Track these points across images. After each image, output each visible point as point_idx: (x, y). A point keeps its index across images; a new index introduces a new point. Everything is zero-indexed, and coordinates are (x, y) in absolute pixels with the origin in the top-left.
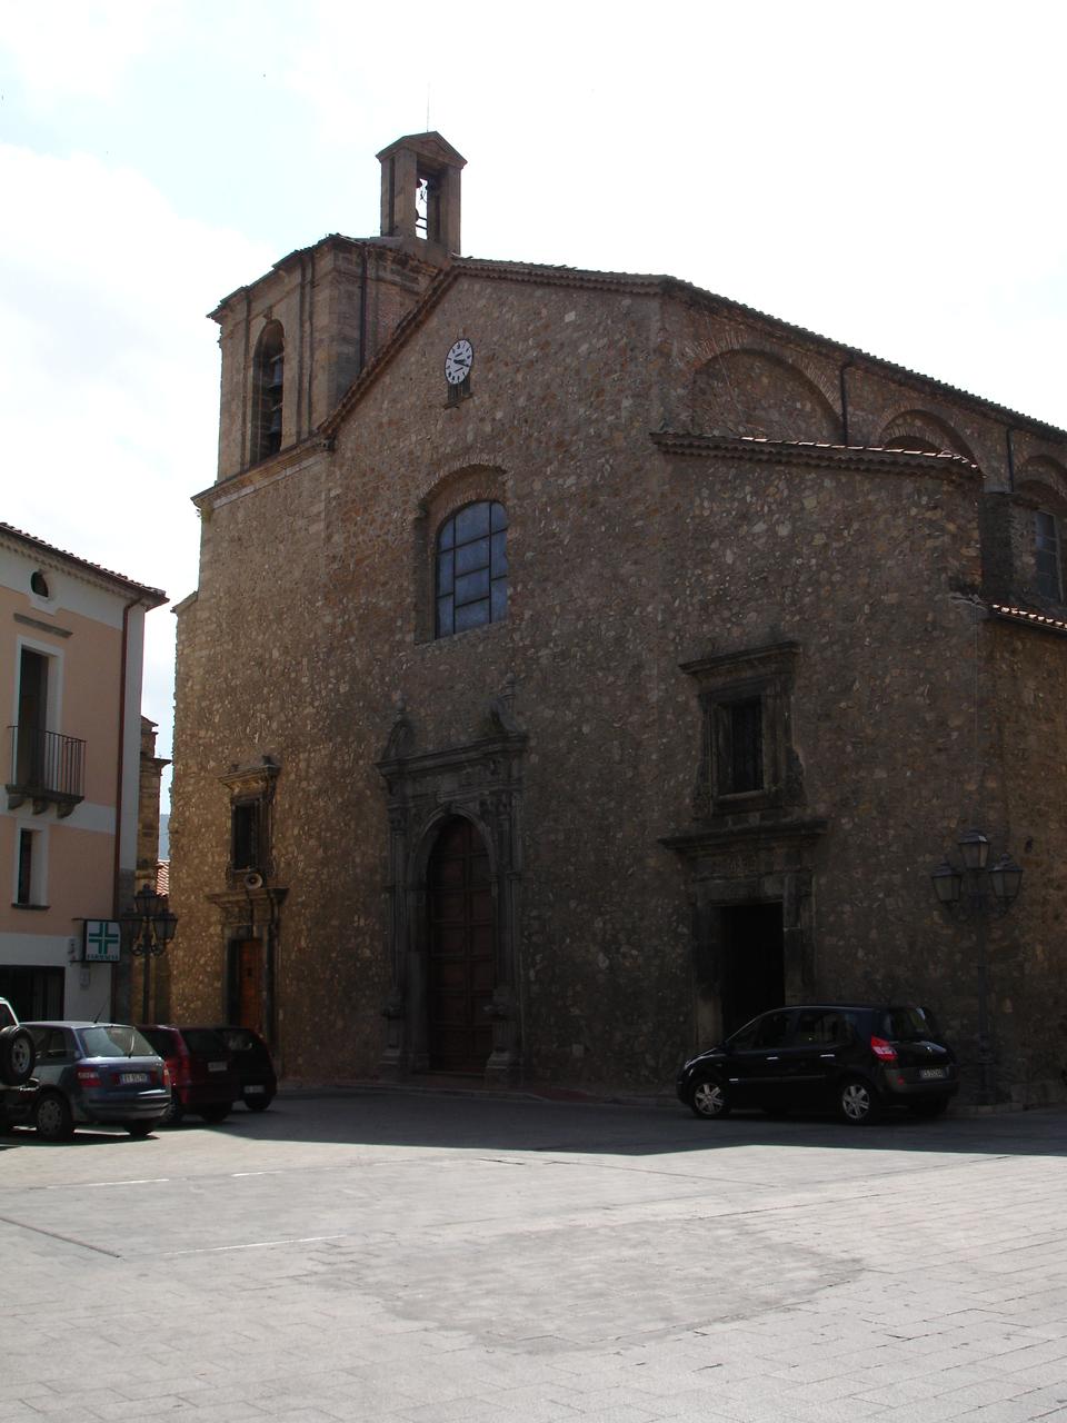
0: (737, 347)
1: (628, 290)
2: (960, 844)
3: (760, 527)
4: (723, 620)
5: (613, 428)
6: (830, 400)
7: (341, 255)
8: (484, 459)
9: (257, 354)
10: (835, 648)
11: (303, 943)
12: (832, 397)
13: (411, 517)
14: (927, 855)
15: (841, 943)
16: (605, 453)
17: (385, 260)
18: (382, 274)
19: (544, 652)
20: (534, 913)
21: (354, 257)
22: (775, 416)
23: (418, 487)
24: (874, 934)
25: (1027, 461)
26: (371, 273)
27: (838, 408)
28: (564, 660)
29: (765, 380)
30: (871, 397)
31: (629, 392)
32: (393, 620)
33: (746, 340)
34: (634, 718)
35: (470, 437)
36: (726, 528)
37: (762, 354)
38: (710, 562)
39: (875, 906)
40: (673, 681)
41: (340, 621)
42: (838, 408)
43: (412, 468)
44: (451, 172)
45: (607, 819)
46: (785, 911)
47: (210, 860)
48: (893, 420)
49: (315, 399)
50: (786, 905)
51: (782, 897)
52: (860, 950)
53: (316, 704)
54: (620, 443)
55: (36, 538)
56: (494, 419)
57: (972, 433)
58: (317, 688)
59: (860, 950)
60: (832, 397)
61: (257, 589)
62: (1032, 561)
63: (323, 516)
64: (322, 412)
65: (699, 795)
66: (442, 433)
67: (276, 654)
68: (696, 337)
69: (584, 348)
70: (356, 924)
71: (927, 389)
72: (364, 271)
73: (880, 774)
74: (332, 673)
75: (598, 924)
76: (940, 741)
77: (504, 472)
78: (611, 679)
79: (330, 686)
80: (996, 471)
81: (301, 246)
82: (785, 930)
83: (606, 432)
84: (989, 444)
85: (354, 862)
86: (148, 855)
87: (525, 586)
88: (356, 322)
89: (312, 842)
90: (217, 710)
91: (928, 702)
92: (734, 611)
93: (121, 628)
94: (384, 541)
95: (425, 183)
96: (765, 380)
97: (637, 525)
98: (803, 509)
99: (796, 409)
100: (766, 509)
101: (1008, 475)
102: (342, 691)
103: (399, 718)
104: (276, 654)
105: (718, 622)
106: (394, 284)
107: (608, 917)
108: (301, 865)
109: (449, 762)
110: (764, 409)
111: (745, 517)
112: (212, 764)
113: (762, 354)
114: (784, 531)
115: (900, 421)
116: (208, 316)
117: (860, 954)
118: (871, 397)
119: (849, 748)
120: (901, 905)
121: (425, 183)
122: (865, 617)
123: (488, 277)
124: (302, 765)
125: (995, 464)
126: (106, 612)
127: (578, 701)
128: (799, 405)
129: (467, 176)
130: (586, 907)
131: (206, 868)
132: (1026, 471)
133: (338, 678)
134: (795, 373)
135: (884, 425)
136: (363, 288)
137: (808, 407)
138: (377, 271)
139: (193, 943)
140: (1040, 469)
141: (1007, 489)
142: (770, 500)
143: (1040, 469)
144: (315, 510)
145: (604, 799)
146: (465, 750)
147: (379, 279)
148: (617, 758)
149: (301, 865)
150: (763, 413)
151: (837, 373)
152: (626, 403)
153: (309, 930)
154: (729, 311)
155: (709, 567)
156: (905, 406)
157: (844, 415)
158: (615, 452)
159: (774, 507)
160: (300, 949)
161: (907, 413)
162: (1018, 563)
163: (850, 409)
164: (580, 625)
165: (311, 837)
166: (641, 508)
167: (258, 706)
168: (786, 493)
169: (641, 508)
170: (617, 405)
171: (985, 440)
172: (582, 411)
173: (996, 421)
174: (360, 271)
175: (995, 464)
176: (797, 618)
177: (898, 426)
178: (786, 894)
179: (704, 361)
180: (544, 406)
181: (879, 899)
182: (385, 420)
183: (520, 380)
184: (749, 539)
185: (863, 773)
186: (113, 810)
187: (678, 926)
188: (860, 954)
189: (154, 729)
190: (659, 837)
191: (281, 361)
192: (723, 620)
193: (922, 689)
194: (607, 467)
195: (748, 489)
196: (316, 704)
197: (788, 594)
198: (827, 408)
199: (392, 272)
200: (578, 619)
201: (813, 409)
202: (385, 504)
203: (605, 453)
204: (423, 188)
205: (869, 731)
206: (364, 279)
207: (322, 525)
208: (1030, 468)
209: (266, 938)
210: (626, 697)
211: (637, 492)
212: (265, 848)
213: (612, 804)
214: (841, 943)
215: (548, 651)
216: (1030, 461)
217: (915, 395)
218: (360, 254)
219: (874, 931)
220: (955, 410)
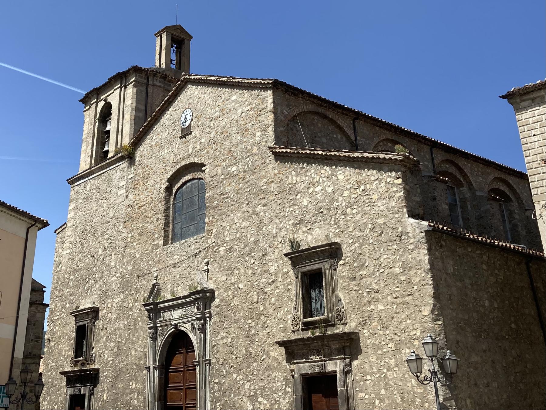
0: (306, 110)
1: (258, 86)
2: (423, 343)
3: (318, 189)
4: (303, 232)
5: (253, 145)
6: (349, 134)
7: (138, 74)
8: (196, 160)
9: (100, 116)
10: (356, 245)
11: (105, 398)
12: (350, 132)
13: (164, 187)
14: (407, 349)
15: (367, 396)
16: (249, 156)
17: (157, 77)
18: (155, 82)
19: (222, 248)
20: (217, 381)
21: (143, 75)
22: (324, 140)
23: (167, 173)
24: (383, 392)
25: (441, 162)
26: (150, 82)
27: (353, 137)
28: (231, 252)
29: (320, 125)
30: (368, 133)
31: (259, 129)
32: (154, 234)
33: (310, 107)
34: (263, 280)
35: (190, 151)
36: (303, 189)
37: (317, 113)
38: (296, 205)
39: (382, 376)
40: (281, 262)
41: (130, 235)
42: (353, 137)
43: (164, 165)
44: (186, 42)
45: (251, 331)
46: (338, 379)
47: (64, 354)
48: (378, 143)
49: (124, 135)
50: (338, 376)
51: (335, 371)
52: (377, 400)
53: (117, 275)
54: (255, 151)
55: (23, 211)
56: (201, 142)
57: (415, 149)
58: (118, 267)
59: (377, 400)
60: (350, 132)
61: (94, 221)
62: (447, 207)
63: (125, 187)
64: (126, 141)
65: (294, 319)
66: (178, 148)
67: (100, 251)
68: (288, 106)
69: (240, 111)
70: (130, 387)
71: (393, 130)
72: (148, 81)
73: (381, 307)
74: (125, 260)
75: (247, 386)
76: (409, 290)
77: (205, 166)
78: (252, 261)
79: (124, 266)
80: (427, 167)
81: (121, 71)
82: (339, 389)
83: (249, 147)
84: (422, 154)
85: (131, 354)
86: (35, 352)
87: (214, 217)
88: (144, 102)
89: (112, 344)
90: (72, 279)
91: (401, 271)
92: (308, 228)
93: (25, 238)
94: (151, 198)
95: (175, 46)
96: (320, 125)
97: (263, 188)
98: (338, 180)
99: (334, 137)
100: (321, 180)
101: (433, 168)
102: (129, 268)
103: (155, 282)
104: (100, 251)
105: (301, 233)
106: (160, 87)
107: (252, 383)
108: (106, 356)
109: (177, 303)
110: (319, 137)
111: (312, 184)
112: (68, 305)
113: (317, 113)
114: (329, 190)
115: (381, 144)
116: (80, 101)
117: (377, 402)
118: (368, 133)
119: (365, 294)
120: (395, 376)
121: (175, 46)
122: (369, 230)
123: (199, 82)
124: (109, 306)
125: (426, 163)
126: (19, 228)
127: (237, 272)
128: (335, 136)
129: (193, 43)
130: (241, 377)
131: (61, 358)
132: (441, 166)
133: (128, 263)
134: (333, 122)
135: (374, 145)
136: (147, 88)
137: (339, 137)
138: (153, 81)
139: (52, 398)
140: (447, 166)
141: (432, 174)
142: (322, 176)
143: (447, 166)
144: (121, 184)
145: (250, 321)
146: (185, 297)
147: (154, 85)
148: (255, 300)
149: (106, 356)
150: (319, 139)
151: (351, 122)
152: (258, 134)
153: (108, 390)
154: (302, 95)
155: (296, 207)
156: (383, 137)
157: (356, 140)
158: (254, 155)
159: (325, 179)
160: (103, 401)
161: (384, 140)
162: (440, 208)
163: (358, 138)
164: (238, 235)
165: (111, 342)
166: (265, 180)
167: (91, 277)
168: (330, 173)
169: (265, 180)
170: (254, 135)
171: (421, 152)
172: (239, 138)
173: (425, 144)
174: (145, 81)
175: (426, 163)
176: (338, 230)
177: (380, 145)
178: (338, 370)
179: (292, 116)
180: (222, 136)
181: (384, 373)
182: (154, 143)
183: (212, 125)
184: (314, 194)
185: (372, 307)
186: (14, 327)
187: (285, 388)
188: (377, 402)
189: (44, 289)
190: (276, 340)
191: (110, 119)
192: (303, 232)
193: (398, 264)
194: (250, 162)
195: (313, 171)
196: (117, 275)
197: (333, 219)
198: (348, 138)
199: (160, 82)
200: (237, 233)
201: (342, 138)
202: (152, 181)
203: (249, 156)
204: (174, 48)
205: (374, 285)
206: (147, 85)
207: (124, 191)
208: (442, 165)
209: (87, 395)
210: (260, 270)
211: (263, 173)
212: (90, 348)
213: (253, 324)
214: (367, 396)
215: (224, 248)
216: (442, 162)
217: (387, 132)
218: (147, 74)
219: (383, 390)
220: (406, 139)
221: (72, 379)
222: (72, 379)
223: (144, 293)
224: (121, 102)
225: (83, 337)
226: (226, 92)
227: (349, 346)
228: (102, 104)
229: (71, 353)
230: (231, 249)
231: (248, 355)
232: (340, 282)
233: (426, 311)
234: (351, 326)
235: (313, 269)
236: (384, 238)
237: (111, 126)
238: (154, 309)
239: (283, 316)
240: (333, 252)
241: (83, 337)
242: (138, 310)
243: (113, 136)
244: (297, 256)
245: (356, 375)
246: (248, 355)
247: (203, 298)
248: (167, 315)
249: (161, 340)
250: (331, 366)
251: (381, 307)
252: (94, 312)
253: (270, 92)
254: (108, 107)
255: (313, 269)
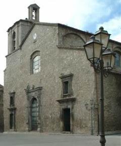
73: (82, 91)
111: (67, 57)
212: (14, 102)
221: (11, 110)
222: (11, 110)
223: (26, 88)
224: (18, 31)
225: (12, 99)
226: (46, 27)
227: (73, 100)
228: (13, 32)
229: (9, 104)
230: (46, 76)
231: (50, 104)
232: (73, 85)
233: (92, 92)
234: (74, 97)
235: (67, 81)
236: (84, 72)
237: (16, 39)
238: (28, 92)
239: (58, 93)
240: (71, 76)
241: (12, 99)
242: (24, 93)
243: (16, 42)
244: (63, 77)
245: (75, 109)
246: (50, 104)
247: (40, 89)
248: (31, 94)
249: (30, 100)
250: (69, 107)
251: (82, 91)
252: (14, 93)
253: (57, 27)
254: (14, 33)
255: (67, 81)
